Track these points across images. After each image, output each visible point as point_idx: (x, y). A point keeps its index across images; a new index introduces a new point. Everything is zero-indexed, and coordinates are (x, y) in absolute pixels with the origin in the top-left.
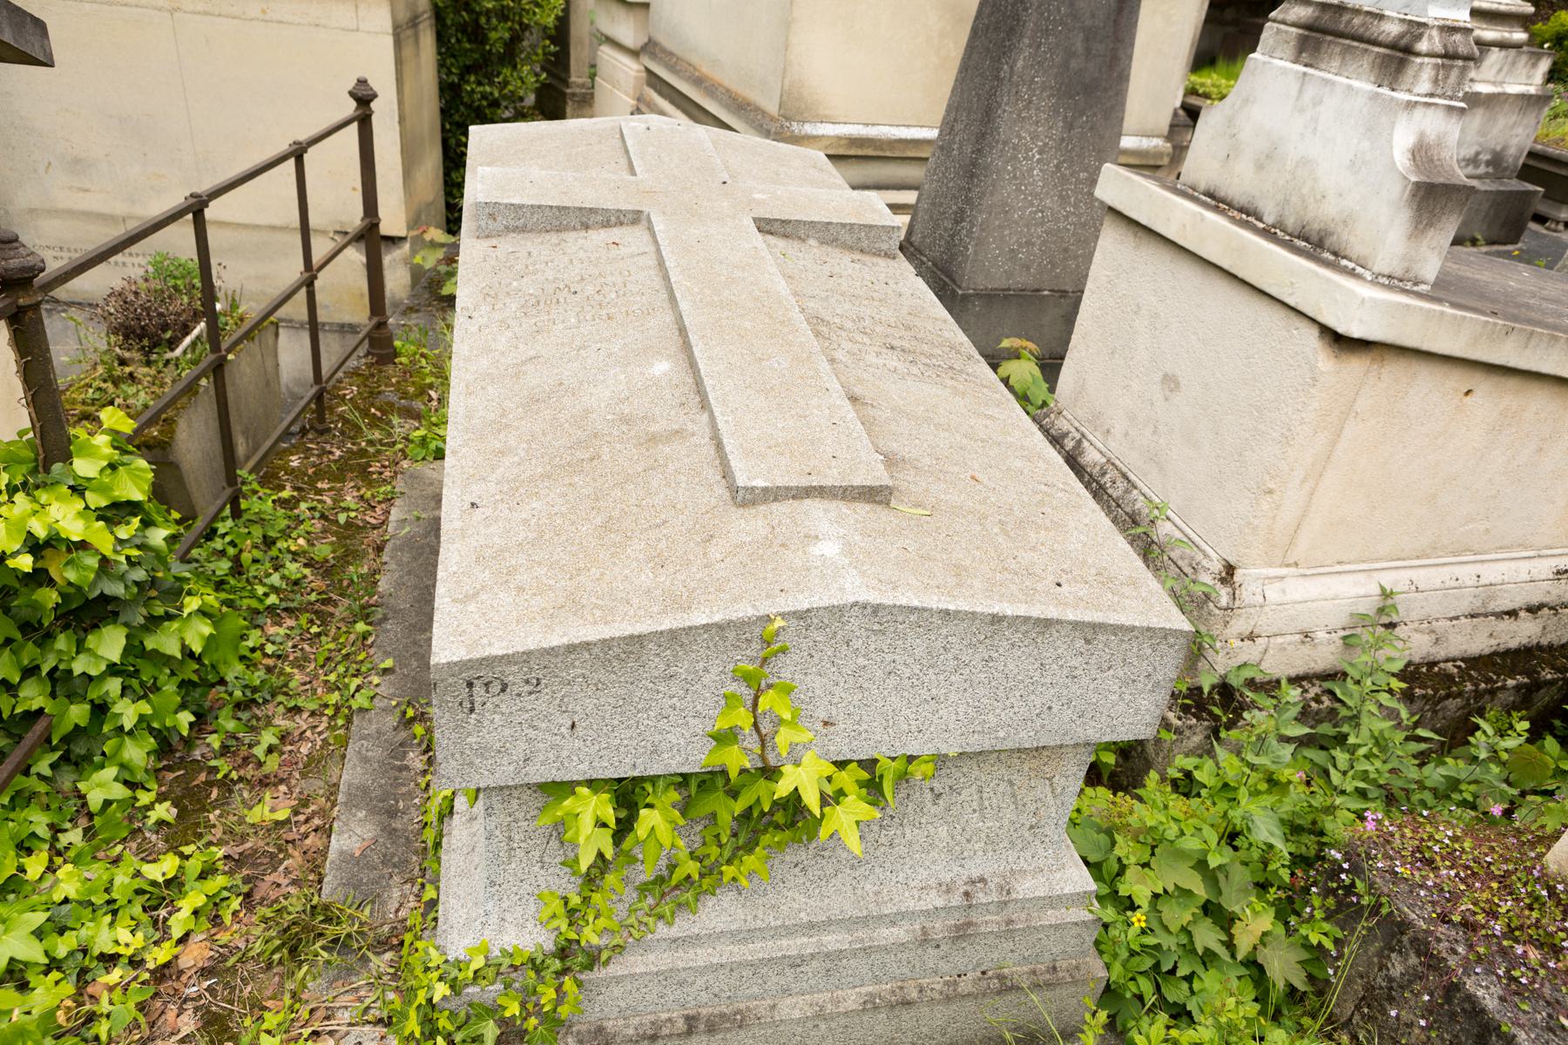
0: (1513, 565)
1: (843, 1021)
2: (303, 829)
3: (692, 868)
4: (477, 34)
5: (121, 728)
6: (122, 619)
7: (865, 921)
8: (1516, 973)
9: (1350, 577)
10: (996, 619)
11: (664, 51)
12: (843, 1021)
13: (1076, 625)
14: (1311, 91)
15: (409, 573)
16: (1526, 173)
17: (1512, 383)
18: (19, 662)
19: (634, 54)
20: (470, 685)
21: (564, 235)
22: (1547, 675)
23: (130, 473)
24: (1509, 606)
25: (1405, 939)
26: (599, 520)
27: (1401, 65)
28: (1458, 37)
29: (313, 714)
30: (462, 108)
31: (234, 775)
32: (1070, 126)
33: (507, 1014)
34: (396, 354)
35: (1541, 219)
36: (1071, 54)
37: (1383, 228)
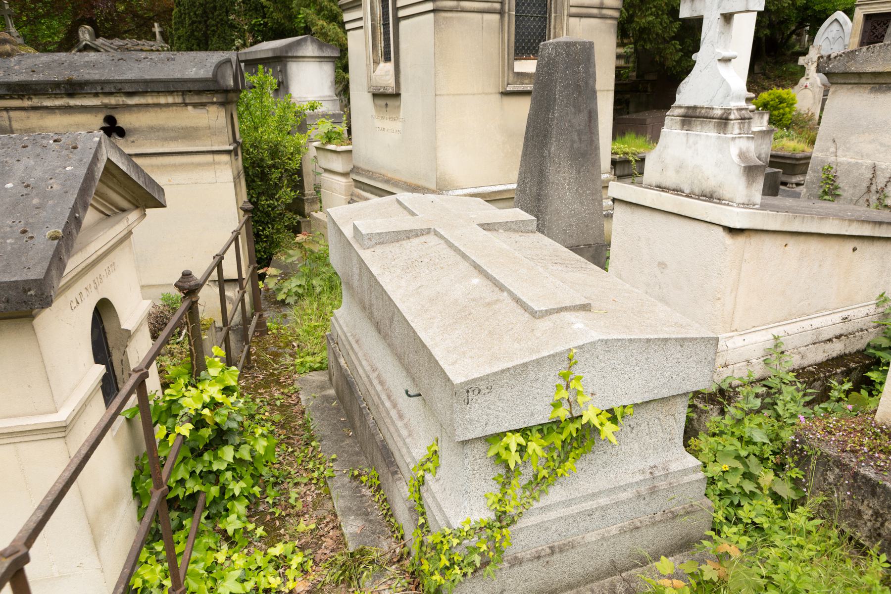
0: (824, 318)
1: (612, 540)
2: (326, 529)
3: (545, 473)
4: (264, 176)
5: (234, 496)
6: (230, 442)
7: (613, 490)
8: (878, 463)
9: (759, 333)
10: (648, 341)
11: (364, 170)
12: (612, 540)
13: (677, 339)
14: (691, 140)
15: (322, 420)
16: (772, 164)
17: (802, 239)
18: (187, 470)
19: (345, 175)
20: (468, 392)
21: (401, 243)
22: (853, 365)
23: (229, 373)
24: (828, 337)
25: (831, 463)
26: (486, 332)
27: (726, 125)
28: (744, 112)
29: (306, 485)
30: (259, 213)
31: (284, 514)
32: (579, 172)
33: (482, 550)
34: (268, 330)
35: (785, 184)
36: (573, 142)
37: (737, 186)
